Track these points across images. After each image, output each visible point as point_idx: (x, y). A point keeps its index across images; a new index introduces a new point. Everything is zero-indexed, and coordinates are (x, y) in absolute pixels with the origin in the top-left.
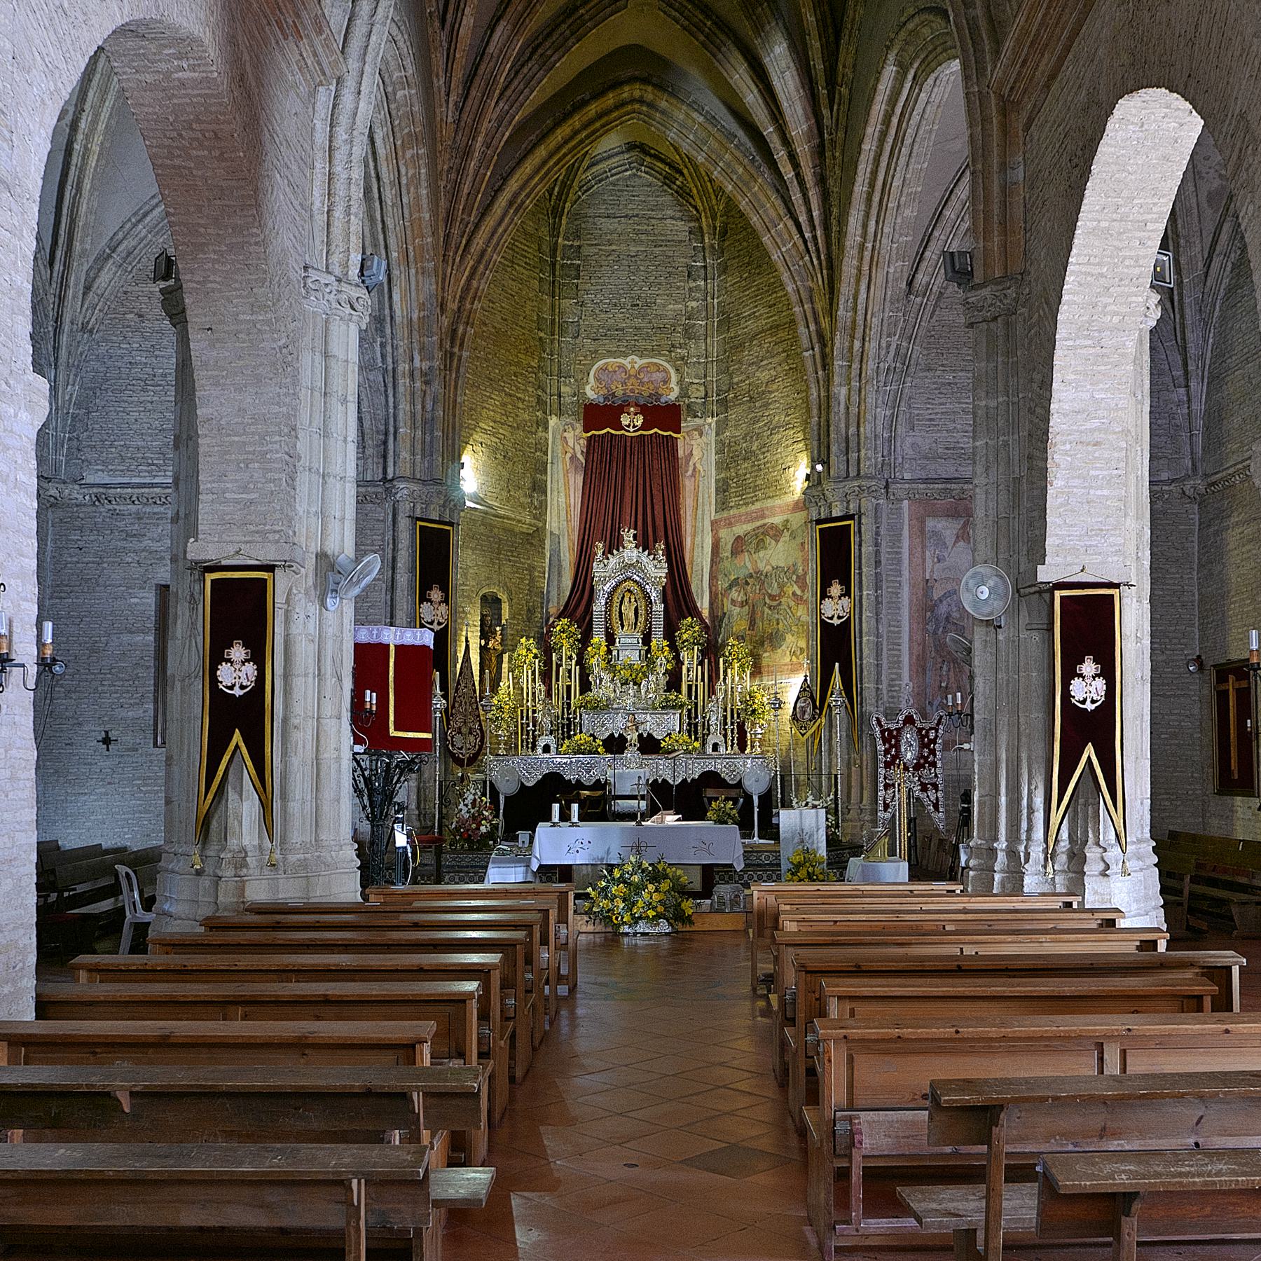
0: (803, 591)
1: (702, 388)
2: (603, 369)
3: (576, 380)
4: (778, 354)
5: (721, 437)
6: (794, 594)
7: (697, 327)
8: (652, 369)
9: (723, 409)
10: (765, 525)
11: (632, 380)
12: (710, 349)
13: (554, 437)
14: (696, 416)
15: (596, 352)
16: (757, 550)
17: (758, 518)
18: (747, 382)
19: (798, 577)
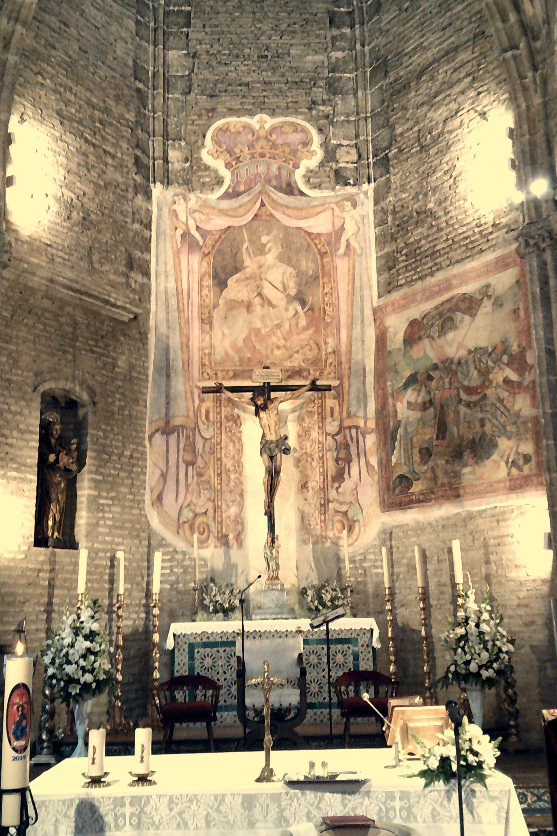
0: (521, 375)
1: (354, 151)
2: (223, 130)
3: (187, 144)
4: (459, 81)
5: (383, 204)
6: (507, 381)
7: (343, 80)
8: (287, 129)
9: (382, 170)
10: (452, 298)
11: (262, 142)
12: (361, 103)
13: (160, 209)
14: (347, 184)
15: (213, 110)
16: (443, 331)
17: (440, 292)
18: (416, 129)
19: (511, 356)
